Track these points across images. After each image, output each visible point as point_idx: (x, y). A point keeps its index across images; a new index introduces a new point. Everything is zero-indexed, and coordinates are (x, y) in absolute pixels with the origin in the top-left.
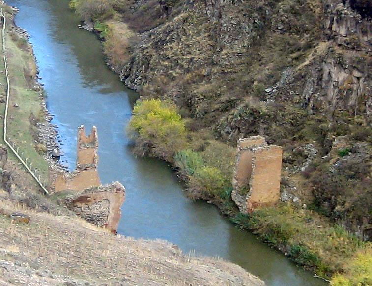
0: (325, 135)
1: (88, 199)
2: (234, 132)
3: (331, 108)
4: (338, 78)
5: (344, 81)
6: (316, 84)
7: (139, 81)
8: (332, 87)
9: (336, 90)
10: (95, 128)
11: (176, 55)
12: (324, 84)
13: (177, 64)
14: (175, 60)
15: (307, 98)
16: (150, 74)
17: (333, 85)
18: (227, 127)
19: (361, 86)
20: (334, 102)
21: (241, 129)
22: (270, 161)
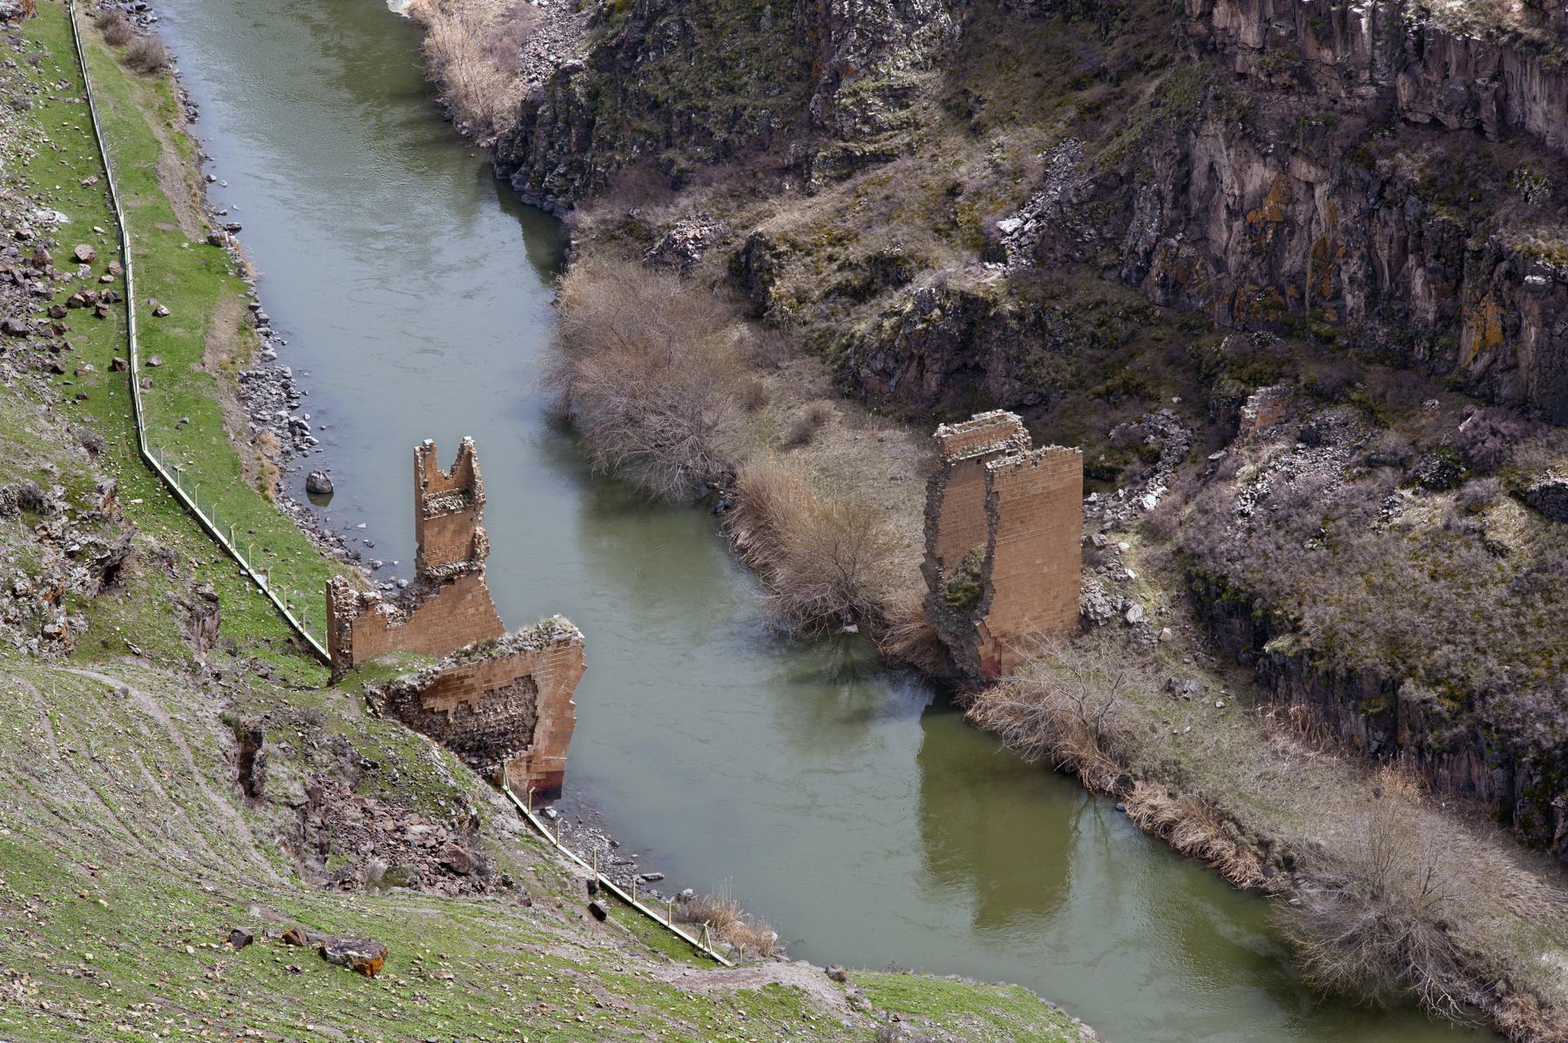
0: (1210, 379)
1: (467, 682)
2: (906, 371)
3: (1226, 282)
4: (1242, 186)
5: (1262, 195)
6: (1168, 205)
7: (559, 182)
8: (1223, 214)
9: (1238, 225)
10: (471, 443)
11: (683, 95)
12: (1196, 204)
13: (688, 130)
14: (680, 114)
15: (1140, 249)
16: (596, 160)
17: (1227, 206)
18: (881, 355)
19: (1323, 213)
20: (1232, 262)
21: (927, 362)
22: (1048, 497)
